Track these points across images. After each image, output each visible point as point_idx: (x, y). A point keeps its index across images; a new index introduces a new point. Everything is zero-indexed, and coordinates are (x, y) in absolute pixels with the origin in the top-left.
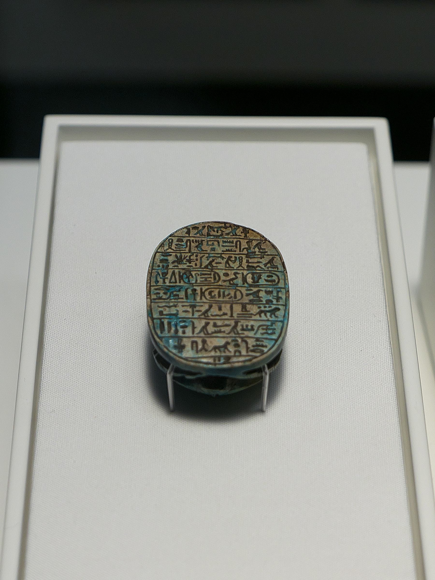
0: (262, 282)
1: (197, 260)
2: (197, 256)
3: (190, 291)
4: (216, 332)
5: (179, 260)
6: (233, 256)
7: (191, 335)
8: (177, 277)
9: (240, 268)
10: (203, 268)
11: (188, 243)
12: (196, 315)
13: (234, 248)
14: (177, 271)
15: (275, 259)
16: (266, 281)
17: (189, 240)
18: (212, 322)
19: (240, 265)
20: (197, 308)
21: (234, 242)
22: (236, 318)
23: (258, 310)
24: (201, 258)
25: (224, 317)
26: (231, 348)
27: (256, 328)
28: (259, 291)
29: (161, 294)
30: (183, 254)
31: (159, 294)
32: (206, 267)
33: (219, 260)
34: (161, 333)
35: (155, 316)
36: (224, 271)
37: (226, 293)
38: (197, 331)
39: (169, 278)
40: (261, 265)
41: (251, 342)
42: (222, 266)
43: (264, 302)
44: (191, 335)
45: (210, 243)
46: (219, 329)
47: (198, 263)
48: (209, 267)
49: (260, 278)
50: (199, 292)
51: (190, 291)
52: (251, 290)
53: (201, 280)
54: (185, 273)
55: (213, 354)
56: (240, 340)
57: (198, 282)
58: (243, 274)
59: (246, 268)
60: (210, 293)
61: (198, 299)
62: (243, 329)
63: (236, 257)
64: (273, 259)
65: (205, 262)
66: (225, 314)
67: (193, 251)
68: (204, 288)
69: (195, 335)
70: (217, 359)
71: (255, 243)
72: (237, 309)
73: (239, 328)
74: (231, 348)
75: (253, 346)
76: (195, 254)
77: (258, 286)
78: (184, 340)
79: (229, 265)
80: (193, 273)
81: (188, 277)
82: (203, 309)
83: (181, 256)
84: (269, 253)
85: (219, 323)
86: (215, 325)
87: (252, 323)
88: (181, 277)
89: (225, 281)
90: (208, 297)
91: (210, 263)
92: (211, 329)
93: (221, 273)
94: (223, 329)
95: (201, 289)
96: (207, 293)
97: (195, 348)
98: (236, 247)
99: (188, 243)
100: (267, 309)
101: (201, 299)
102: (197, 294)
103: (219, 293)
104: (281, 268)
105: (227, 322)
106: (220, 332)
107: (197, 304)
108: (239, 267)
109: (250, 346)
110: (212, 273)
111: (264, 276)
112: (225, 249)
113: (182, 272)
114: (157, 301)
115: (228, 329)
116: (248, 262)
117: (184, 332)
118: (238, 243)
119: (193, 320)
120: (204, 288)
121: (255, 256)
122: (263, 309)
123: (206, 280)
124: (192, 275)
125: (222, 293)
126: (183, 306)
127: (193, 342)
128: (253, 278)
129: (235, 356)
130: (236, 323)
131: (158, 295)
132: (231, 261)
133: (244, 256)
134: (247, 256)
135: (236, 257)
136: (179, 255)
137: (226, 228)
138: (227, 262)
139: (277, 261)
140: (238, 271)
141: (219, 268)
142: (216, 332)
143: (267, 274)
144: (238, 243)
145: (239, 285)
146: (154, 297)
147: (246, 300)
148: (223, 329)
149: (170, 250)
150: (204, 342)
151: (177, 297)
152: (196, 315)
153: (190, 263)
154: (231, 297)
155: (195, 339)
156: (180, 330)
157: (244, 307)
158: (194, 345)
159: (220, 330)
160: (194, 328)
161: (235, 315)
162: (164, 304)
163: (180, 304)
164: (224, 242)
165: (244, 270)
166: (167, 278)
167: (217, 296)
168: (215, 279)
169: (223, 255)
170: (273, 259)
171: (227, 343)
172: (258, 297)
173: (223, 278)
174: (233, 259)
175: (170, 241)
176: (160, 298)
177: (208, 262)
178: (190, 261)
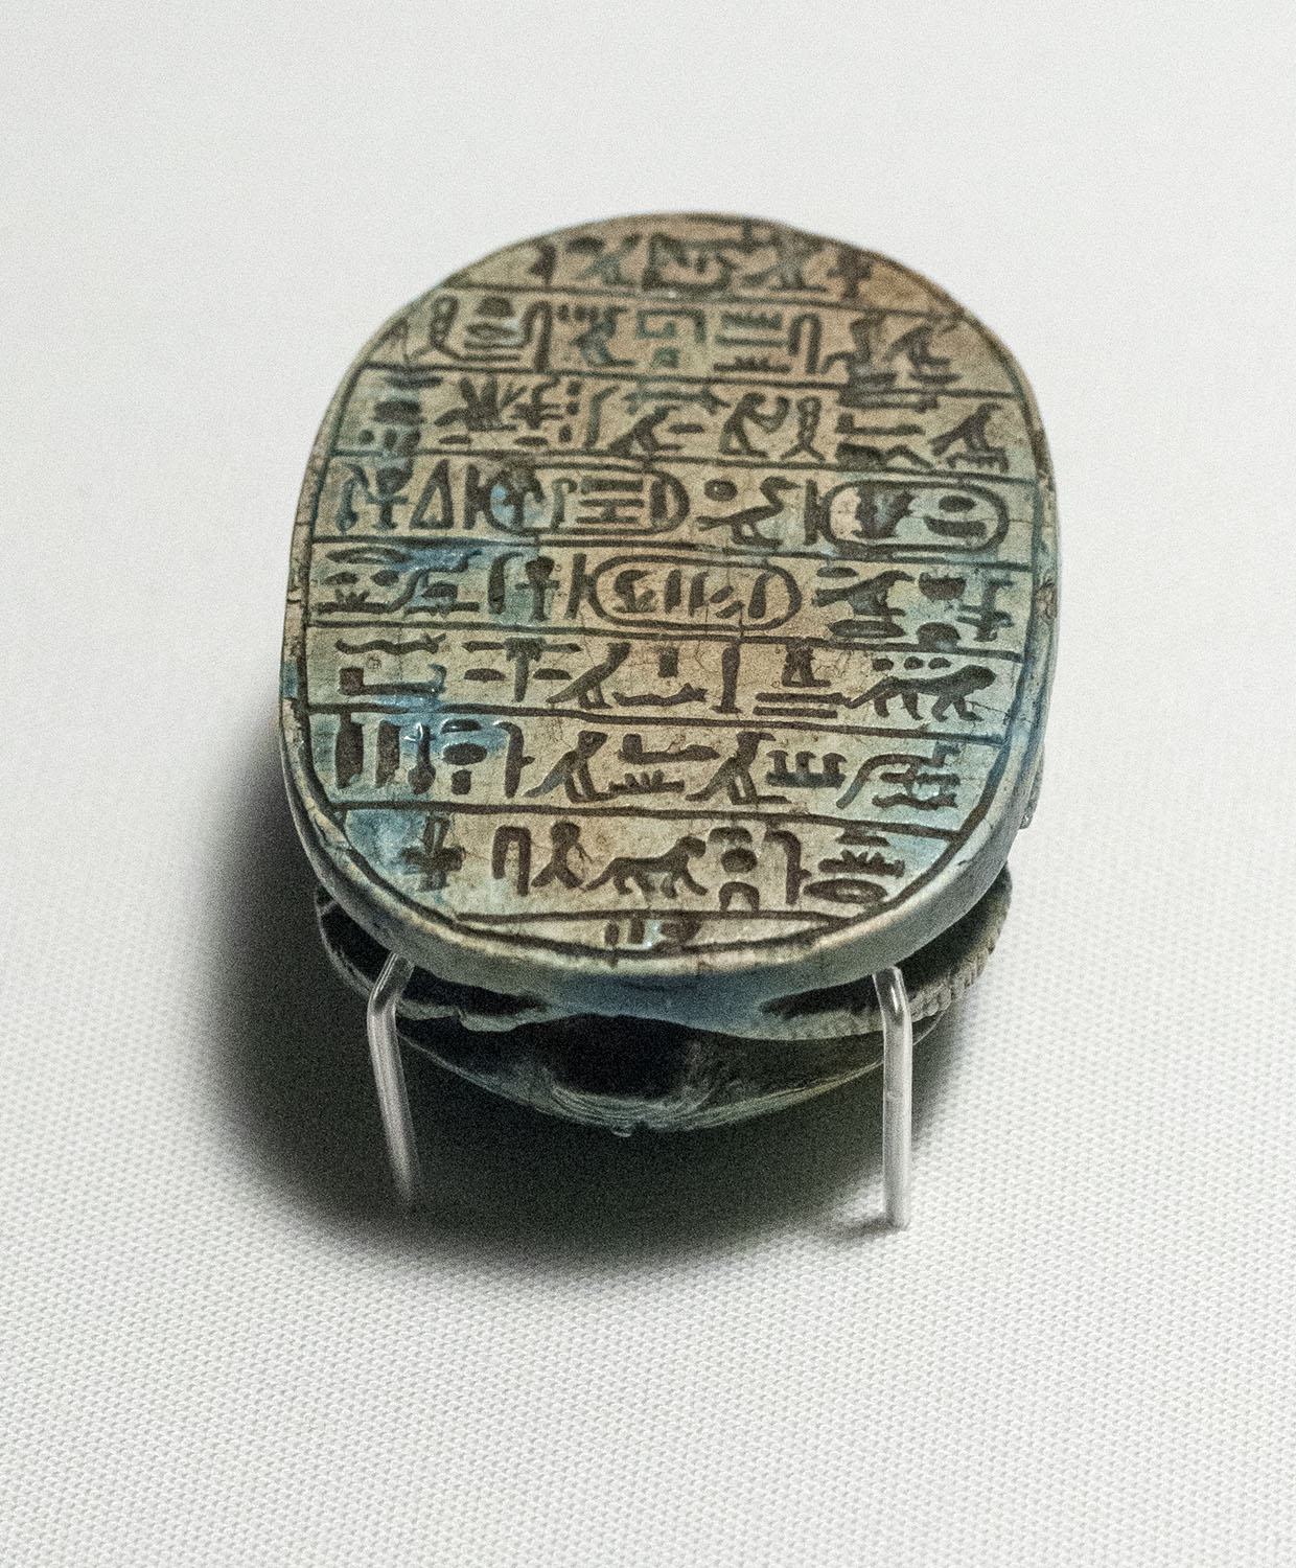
0: (912, 531)
1: (573, 409)
2: (574, 389)
3: (516, 572)
5: (480, 410)
6: (771, 393)
8: (459, 494)
9: (803, 457)
10: (600, 454)
11: (538, 324)
13: (780, 355)
14: (459, 464)
15: (996, 417)
16: (935, 525)
17: (545, 307)
18: (616, 735)
19: (805, 444)
20: (548, 660)
22: (748, 715)
23: (876, 678)
24: (598, 399)
25: (681, 710)
26: (708, 871)
27: (850, 773)
28: (889, 578)
29: (365, 584)
31: (351, 579)
32: (620, 447)
33: (694, 413)
34: (343, 784)
35: (318, 694)
36: (713, 473)
37: (712, 585)
38: (531, 776)
39: (415, 498)
40: (920, 446)
42: (705, 445)
43: (913, 639)
44: (499, 796)
45: (655, 324)
46: (651, 769)
47: (579, 425)
48: (637, 449)
49: (901, 510)
50: (564, 574)
51: (516, 572)
52: (849, 573)
53: (586, 512)
54: (502, 478)
55: (606, 897)
56: (757, 829)
57: (569, 522)
58: (812, 488)
59: (831, 459)
60: (624, 585)
61: (557, 611)
62: (781, 777)
63: (783, 402)
64: (983, 416)
66: (693, 694)
67: (556, 361)
68: (595, 557)
71: (895, 329)
73: (761, 768)
74: (708, 871)
75: (827, 865)
76: (565, 380)
77: (886, 552)
78: (460, 819)
79: (743, 439)
80: (546, 478)
81: (516, 500)
82: (579, 665)
83: (492, 387)
84: (966, 383)
85: (655, 739)
86: (633, 751)
87: (832, 743)
89: (711, 523)
90: (611, 601)
91: (644, 430)
92: (607, 768)
93: (696, 481)
94: (672, 771)
95: (580, 562)
96: (606, 583)
97: (512, 870)
98: (794, 348)
99: (538, 324)
100: (924, 674)
101: (573, 609)
103: (674, 582)
104: (1022, 464)
105: (697, 737)
106: (657, 785)
108: (796, 451)
109: (810, 863)
111: (926, 504)
112: (729, 355)
113: (488, 469)
115: (698, 773)
116: (845, 425)
117: (462, 783)
118: (807, 327)
119: (516, 720)
120: (595, 557)
121: (890, 398)
122: (899, 671)
123: (610, 517)
124: (536, 487)
126: (471, 647)
127: (506, 834)
128: (865, 512)
129: (724, 914)
130: (749, 744)
131: (346, 589)
132: (759, 420)
133: (828, 398)
134: (849, 395)
135: (783, 402)
136: (480, 381)
137: (749, 246)
138: (734, 427)
139: (1005, 429)
140: (789, 475)
142: (632, 787)
144: (807, 327)
146: (322, 594)
147: (813, 622)
148: (672, 771)
149: (435, 357)
150: (566, 835)
151: (445, 601)
152: (539, 693)
153: (534, 425)
156: (445, 772)
157: (799, 659)
160: (518, 760)
161: (746, 701)
162: (371, 635)
163: (457, 638)
164: (729, 319)
166: (404, 501)
168: (658, 508)
169: (718, 390)
170: (983, 416)
171: (692, 846)
173: (702, 505)
174: (768, 409)
175: (444, 308)
176: (358, 603)
177: (634, 420)
178: (534, 414)
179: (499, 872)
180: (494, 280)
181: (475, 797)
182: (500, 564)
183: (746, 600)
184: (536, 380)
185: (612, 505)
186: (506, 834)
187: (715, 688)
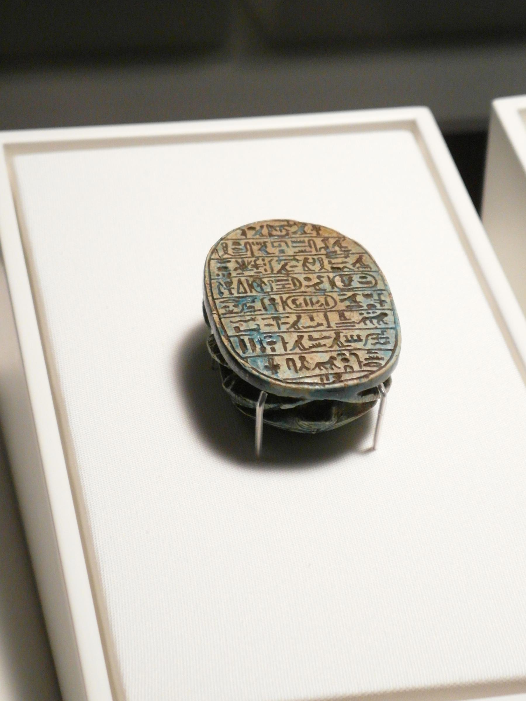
4: (314, 346)
7: (283, 352)
9: (323, 270)
12: (284, 328)
14: (243, 279)
17: (248, 243)
21: (307, 241)
22: (335, 328)
23: (361, 317)
29: (231, 308)
30: (246, 260)
31: (228, 307)
32: (279, 272)
34: (244, 353)
38: (290, 346)
40: (348, 265)
41: (363, 355)
44: (283, 352)
55: (317, 371)
56: (347, 354)
57: (275, 290)
60: (294, 301)
65: (277, 267)
66: (319, 325)
69: (288, 352)
70: (324, 378)
72: (334, 318)
74: (338, 363)
80: (265, 280)
85: (315, 335)
86: (311, 338)
88: (251, 286)
90: (293, 306)
92: (306, 343)
93: (301, 278)
94: (322, 342)
96: (289, 302)
97: (292, 368)
98: (311, 247)
101: (284, 309)
102: (278, 303)
106: (319, 345)
107: (281, 315)
110: (290, 279)
111: (356, 278)
114: (227, 315)
116: (330, 263)
118: (312, 242)
120: (285, 297)
122: (366, 315)
124: (264, 282)
125: (308, 301)
127: (288, 360)
129: (346, 372)
130: (338, 334)
131: (227, 309)
134: (328, 256)
135: (313, 259)
136: (240, 260)
137: (290, 226)
140: (322, 275)
141: (296, 272)
142: (314, 346)
143: (359, 276)
145: (328, 290)
151: (252, 310)
153: (257, 268)
154: (322, 304)
155: (291, 357)
156: (268, 348)
157: (341, 315)
158: (291, 364)
159: (319, 343)
165: (328, 272)
166: (233, 288)
167: (303, 304)
168: (295, 285)
171: (332, 358)
172: (355, 301)
173: (305, 283)
176: (231, 312)
178: (256, 266)
179: (289, 369)
180: (233, 238)
181: (277, 352)
182: (262, 300)
183: (324, 303)
184: (254, 259)
185: (283, 285)
186: (288, 360)
187: (325, 322)
